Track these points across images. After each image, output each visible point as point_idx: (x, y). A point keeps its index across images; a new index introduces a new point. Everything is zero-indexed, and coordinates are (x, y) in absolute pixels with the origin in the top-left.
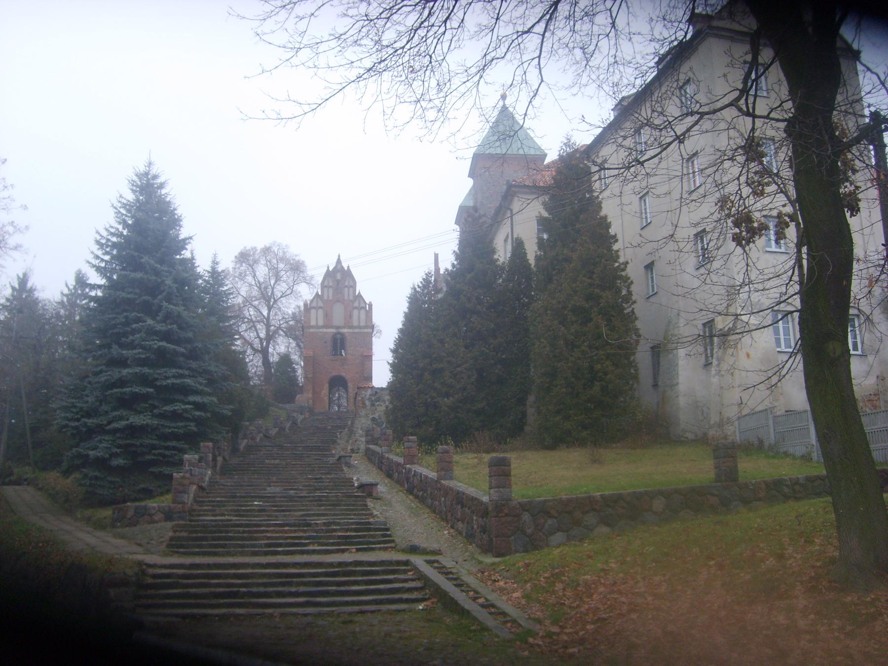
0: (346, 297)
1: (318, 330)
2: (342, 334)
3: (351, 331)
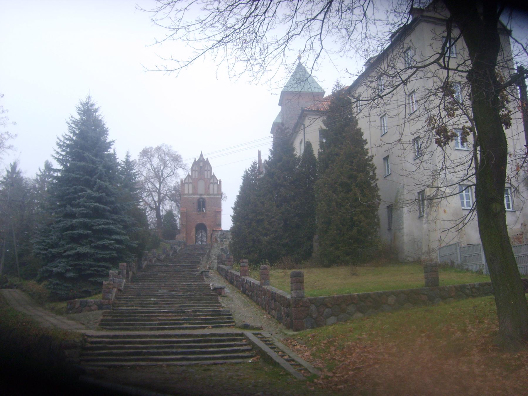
0: (206, 177)
1: (189, 196)
2: (203, 199)
3: (209, 197)
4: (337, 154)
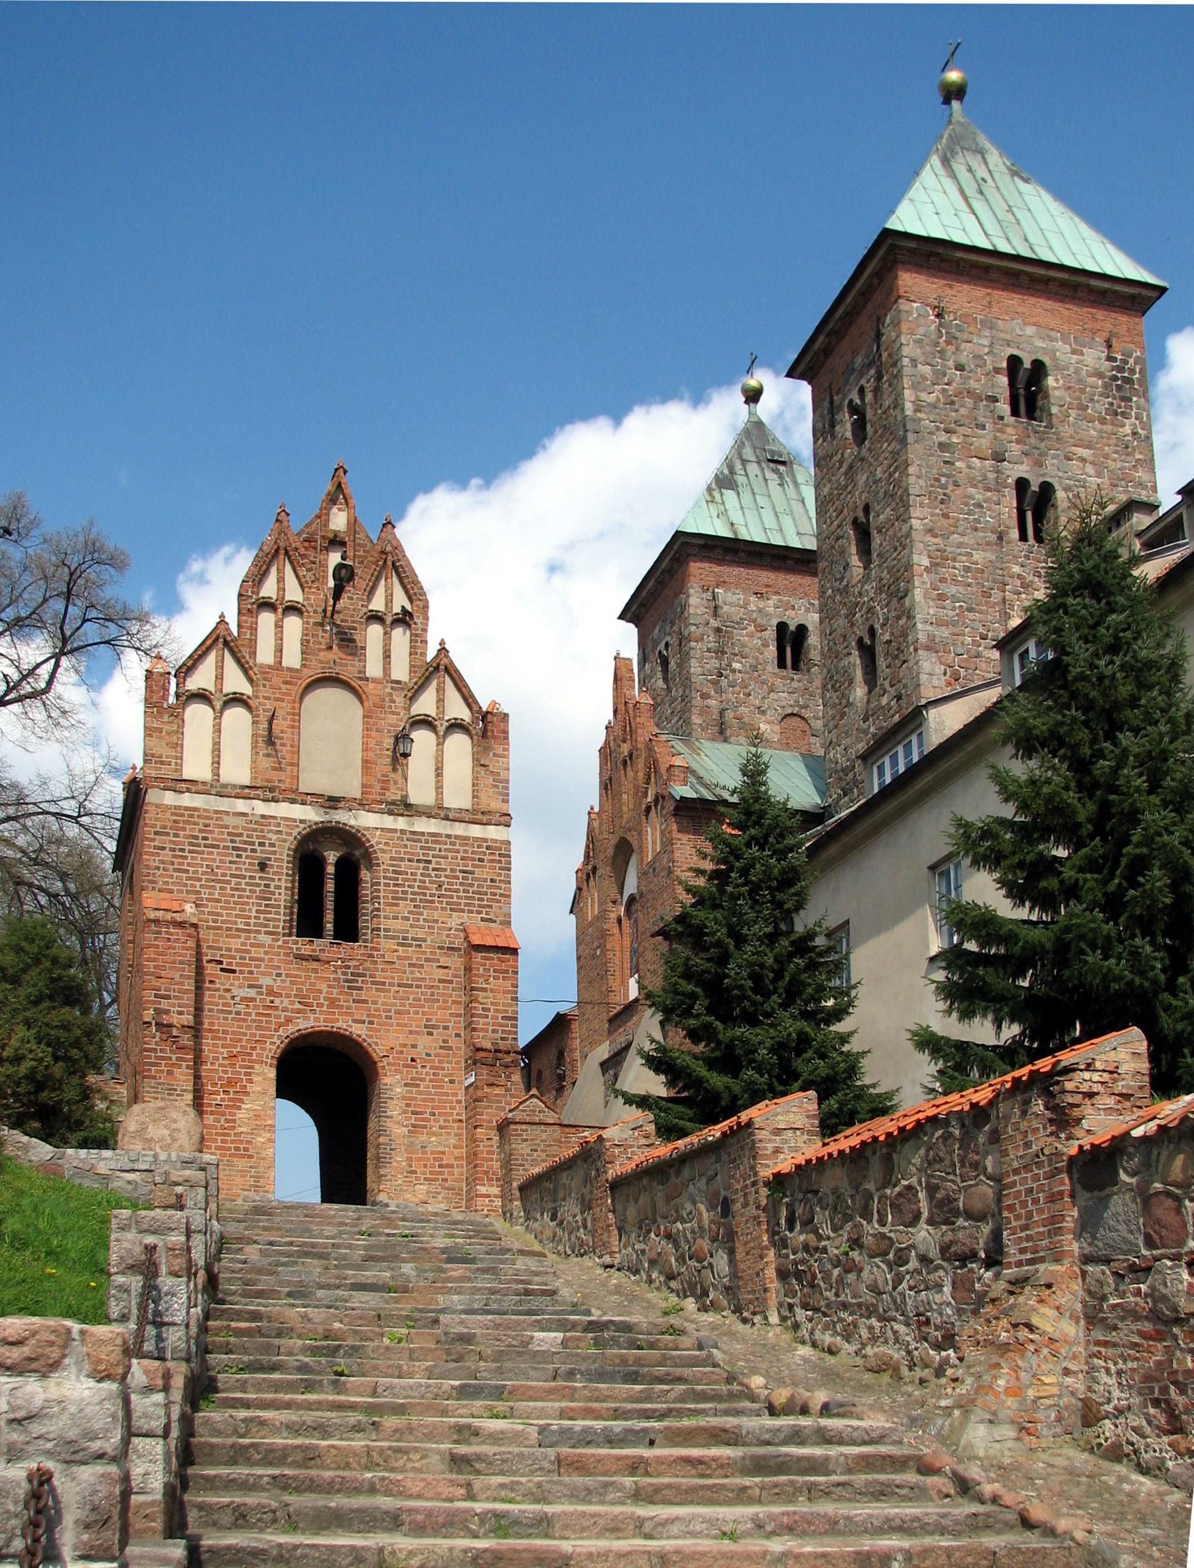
0: (374, 668)
1: (224, 804)
2: (349, 839)
3: (401, 823)
4: (1062, 723)
